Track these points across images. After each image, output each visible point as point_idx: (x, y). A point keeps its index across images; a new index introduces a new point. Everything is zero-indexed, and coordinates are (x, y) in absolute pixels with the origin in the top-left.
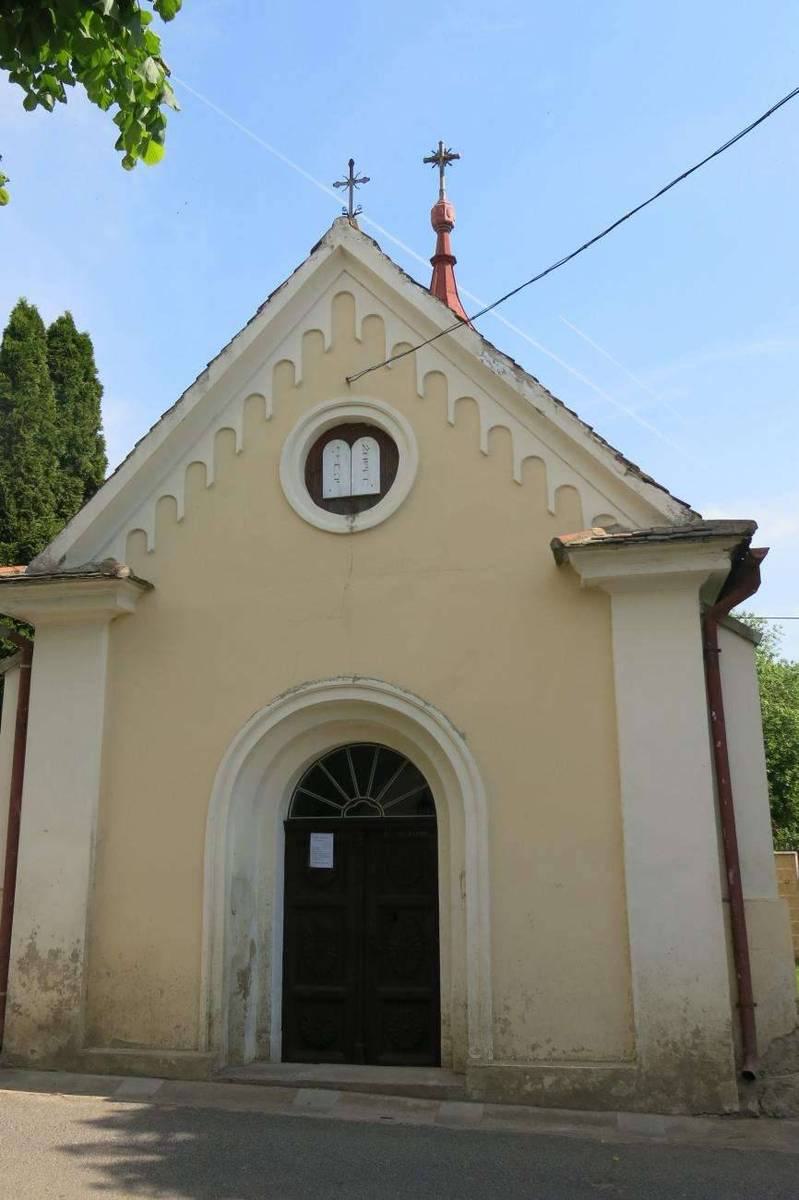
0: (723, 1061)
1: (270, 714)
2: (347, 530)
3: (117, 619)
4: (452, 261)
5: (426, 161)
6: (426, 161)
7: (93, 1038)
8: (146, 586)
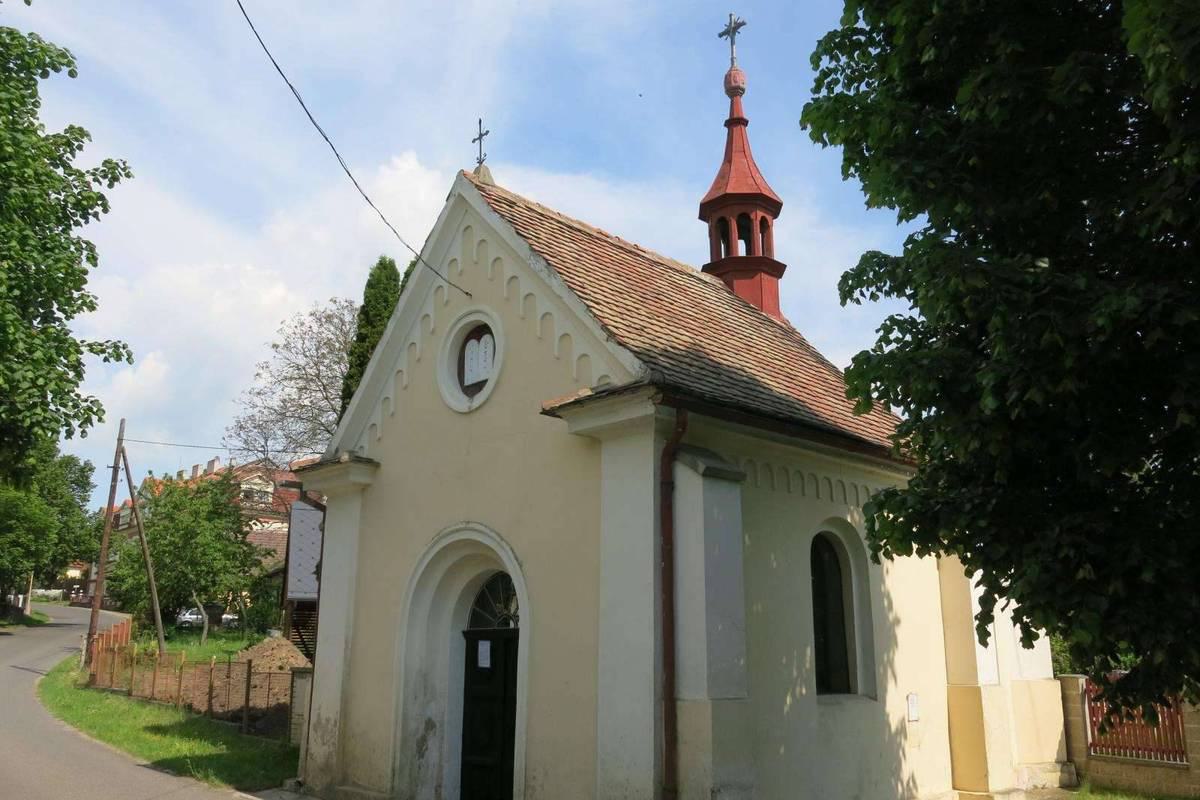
0: (300, 779)
1: (427, 553)
2: (466, 410)
3: (364, 489)
4: (745, 122)
5: (720, 35)
6: (720, 35)
7: (344, 781)
8: (372, 463)
